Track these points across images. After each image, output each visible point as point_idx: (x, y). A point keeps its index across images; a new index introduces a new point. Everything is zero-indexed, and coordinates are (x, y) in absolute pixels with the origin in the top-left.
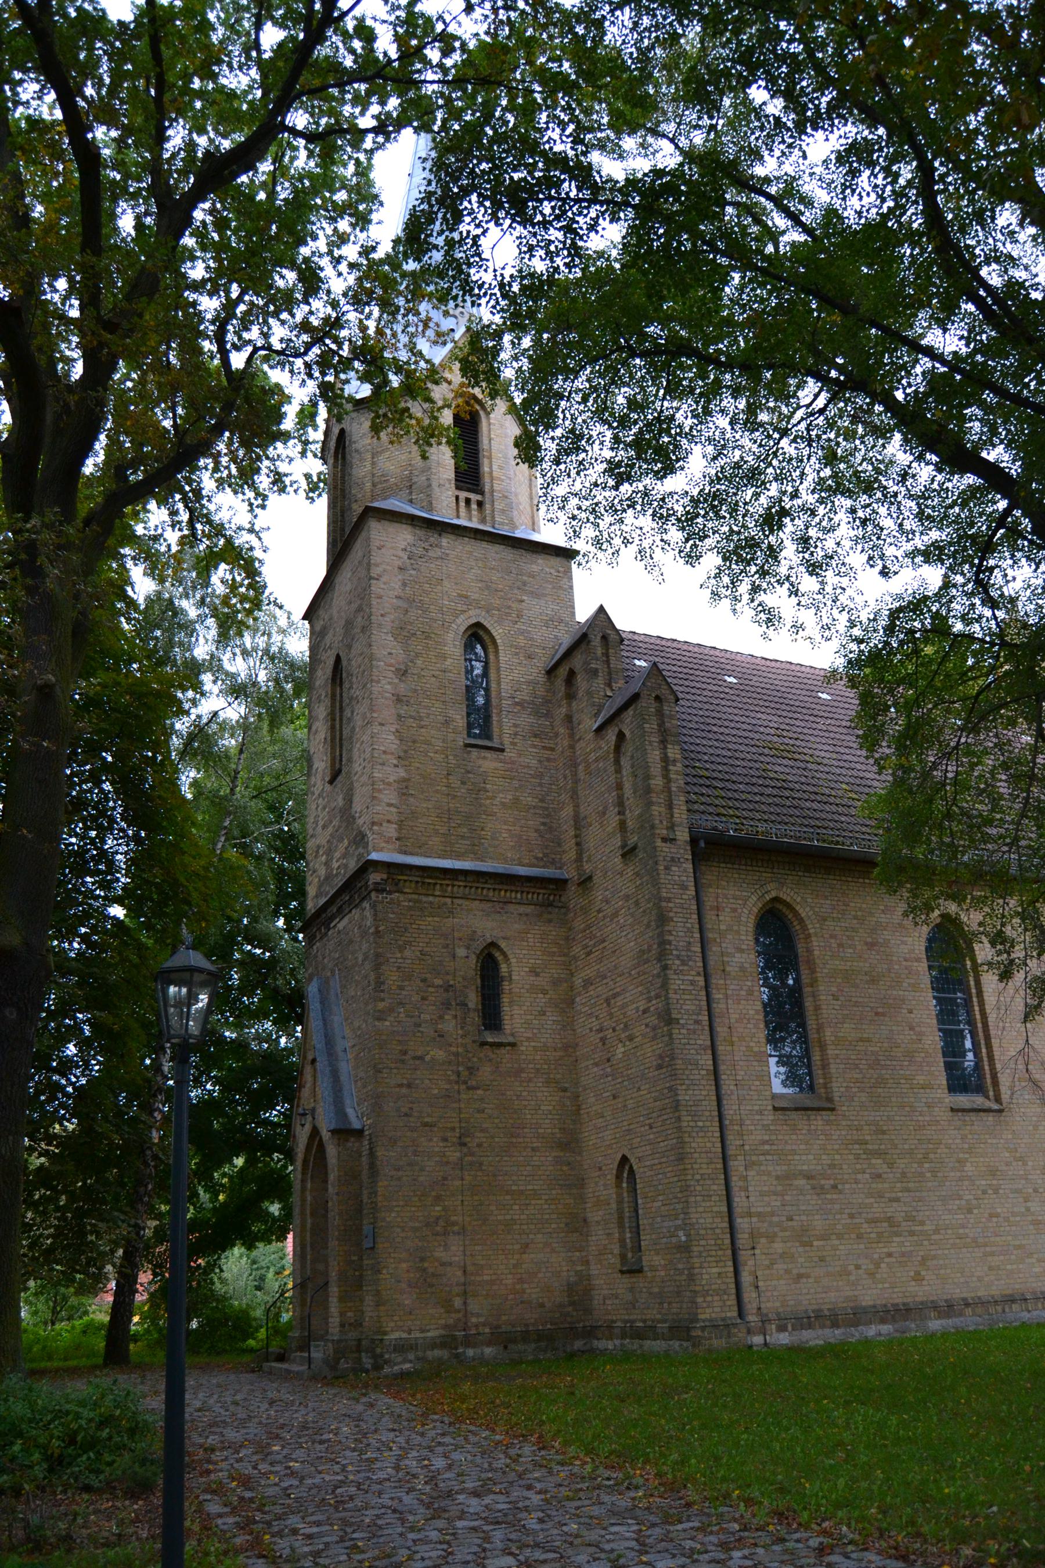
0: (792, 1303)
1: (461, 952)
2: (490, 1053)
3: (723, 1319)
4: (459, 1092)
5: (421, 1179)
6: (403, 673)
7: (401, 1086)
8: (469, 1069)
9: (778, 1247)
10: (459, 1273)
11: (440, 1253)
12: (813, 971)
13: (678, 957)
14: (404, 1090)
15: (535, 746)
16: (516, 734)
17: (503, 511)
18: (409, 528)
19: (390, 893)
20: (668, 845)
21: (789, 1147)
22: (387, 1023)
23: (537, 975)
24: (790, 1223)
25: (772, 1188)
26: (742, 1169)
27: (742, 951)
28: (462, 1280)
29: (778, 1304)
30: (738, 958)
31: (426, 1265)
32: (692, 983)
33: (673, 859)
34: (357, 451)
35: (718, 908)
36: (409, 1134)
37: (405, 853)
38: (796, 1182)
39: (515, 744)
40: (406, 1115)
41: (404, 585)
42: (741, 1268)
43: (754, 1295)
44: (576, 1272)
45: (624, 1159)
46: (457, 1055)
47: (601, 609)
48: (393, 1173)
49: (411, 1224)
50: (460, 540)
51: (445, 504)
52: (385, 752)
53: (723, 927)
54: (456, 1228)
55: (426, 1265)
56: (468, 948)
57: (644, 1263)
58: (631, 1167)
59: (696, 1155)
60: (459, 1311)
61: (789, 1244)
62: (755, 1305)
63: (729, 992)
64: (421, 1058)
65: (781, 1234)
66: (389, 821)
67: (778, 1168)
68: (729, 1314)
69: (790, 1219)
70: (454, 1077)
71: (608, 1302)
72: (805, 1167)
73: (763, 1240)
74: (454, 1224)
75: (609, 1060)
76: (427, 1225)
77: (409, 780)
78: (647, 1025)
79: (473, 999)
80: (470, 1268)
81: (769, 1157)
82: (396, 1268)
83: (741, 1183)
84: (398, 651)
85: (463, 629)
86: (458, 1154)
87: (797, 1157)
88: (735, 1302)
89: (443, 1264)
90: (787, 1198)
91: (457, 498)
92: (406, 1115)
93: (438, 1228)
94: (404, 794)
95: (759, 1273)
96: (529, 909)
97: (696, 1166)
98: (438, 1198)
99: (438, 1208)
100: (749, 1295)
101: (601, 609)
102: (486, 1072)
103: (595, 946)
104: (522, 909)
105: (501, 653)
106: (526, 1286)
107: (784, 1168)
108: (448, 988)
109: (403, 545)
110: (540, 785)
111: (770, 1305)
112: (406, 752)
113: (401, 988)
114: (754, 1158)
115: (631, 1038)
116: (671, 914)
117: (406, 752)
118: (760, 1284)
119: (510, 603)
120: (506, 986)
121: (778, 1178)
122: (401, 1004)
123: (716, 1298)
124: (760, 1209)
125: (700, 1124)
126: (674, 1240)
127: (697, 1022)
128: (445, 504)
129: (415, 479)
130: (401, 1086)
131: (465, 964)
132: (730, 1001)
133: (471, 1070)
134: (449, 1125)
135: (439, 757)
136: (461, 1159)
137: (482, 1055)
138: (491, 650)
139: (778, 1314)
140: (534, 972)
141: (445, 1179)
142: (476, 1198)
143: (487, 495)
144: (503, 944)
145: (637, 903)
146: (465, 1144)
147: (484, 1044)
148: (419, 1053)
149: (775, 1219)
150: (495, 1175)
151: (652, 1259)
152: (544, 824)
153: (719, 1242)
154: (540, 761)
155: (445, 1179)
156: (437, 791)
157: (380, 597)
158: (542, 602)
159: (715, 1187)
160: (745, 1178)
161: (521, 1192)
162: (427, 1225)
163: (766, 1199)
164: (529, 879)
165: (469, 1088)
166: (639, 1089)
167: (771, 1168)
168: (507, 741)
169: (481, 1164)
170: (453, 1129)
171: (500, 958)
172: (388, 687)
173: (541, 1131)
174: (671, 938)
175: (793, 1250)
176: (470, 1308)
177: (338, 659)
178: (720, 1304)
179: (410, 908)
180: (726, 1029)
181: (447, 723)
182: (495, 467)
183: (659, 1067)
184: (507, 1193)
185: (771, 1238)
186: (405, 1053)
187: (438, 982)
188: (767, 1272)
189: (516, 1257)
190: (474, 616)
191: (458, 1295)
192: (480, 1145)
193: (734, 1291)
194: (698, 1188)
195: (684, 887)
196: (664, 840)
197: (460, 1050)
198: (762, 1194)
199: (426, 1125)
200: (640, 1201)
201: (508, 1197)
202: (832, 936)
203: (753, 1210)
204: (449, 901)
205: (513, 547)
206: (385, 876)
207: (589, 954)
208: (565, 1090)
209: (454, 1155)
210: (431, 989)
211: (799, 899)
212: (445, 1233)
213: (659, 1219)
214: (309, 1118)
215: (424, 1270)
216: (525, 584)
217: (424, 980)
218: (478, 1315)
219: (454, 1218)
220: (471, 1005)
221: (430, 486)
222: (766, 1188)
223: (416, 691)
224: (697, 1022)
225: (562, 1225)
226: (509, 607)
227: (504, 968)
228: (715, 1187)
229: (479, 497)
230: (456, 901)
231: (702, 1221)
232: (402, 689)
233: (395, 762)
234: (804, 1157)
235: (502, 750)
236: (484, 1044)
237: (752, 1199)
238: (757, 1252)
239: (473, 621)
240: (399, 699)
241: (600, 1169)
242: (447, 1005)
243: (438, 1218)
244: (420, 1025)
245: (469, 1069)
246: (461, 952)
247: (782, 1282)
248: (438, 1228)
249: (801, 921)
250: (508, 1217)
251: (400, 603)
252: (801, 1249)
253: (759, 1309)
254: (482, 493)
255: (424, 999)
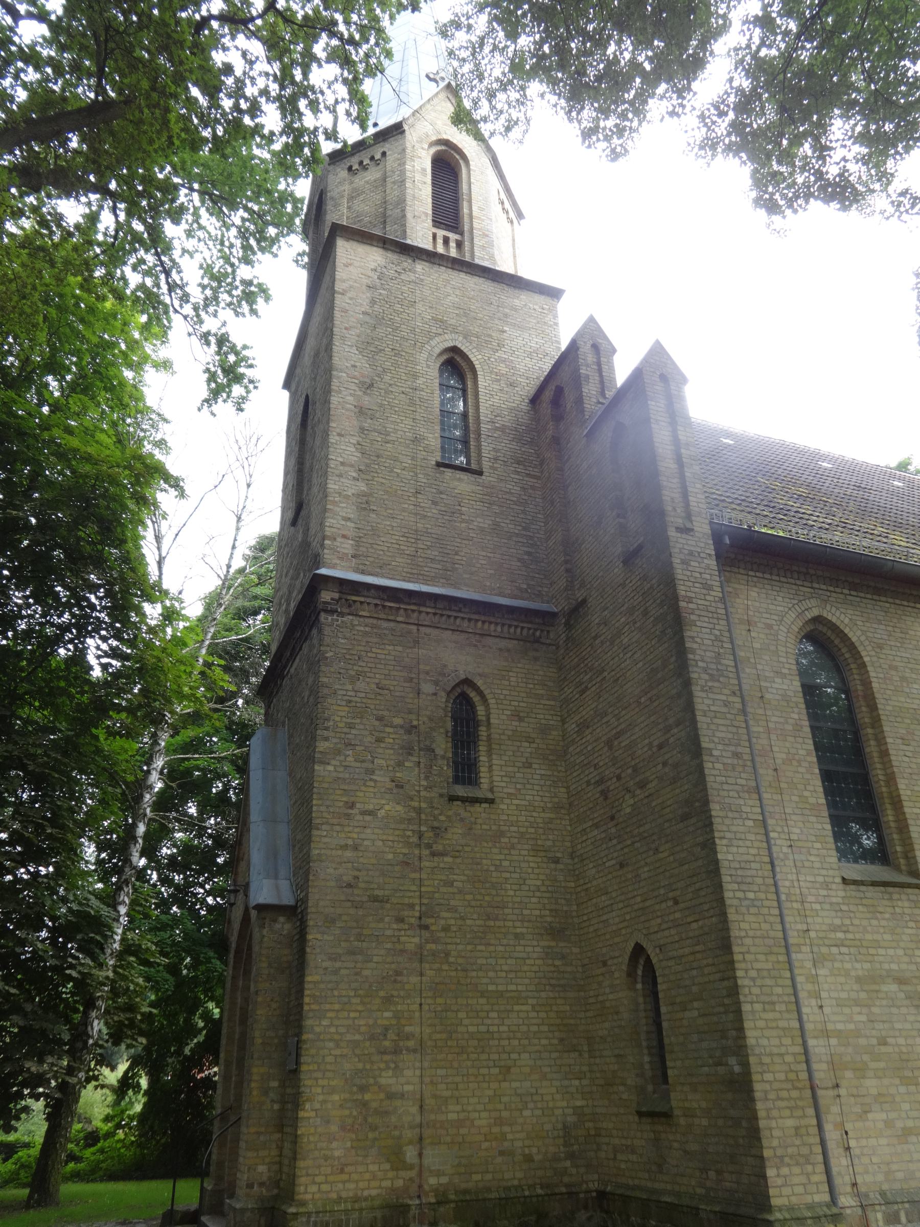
0: (900, 1175)
1: (427, 688)
2: (461, 811)
3: (810, 1207)
4: (420, 858)
5: (366, 973)
6: (368, 387)
7: (345, 847)
8: (433, 828)
9: (871, 1085)
10: (414, 1110)
11: (387, 1079)
12: (873, 707)
13: (705, 670)
14: (349, 854)
15: (518, 473)
16: (496, 459)
17: (483, 248)
18: (381, 251)
19: (342, 614)
20: (684, 536)
21: (869, 937)
22: (331, 768)
23: (521, 719)
24: (883, 1049)
25: (853, 995)
26: (809, 964)
27: (784, 676)
28: (418, 1119)
29: (880, 1177)
30: (779, 683)
31: (367, 1097)
32: (726, 704)
33: (691, 553)
34: (332, 198)
35: (749, 623)
36: (352, 911)
37: (363, 572)
38: (884, 988)
39: (495, 469)
40: (349, 886)
41: (373, 302)
42: (823, 1117)
43: (844, 1162)
44: (574, 1108)
45: (639, 950)
46: (419, 811)
47: (591, 320)
48: (327, 964)
49: (349, 1037)
50: (436, 268)
51: (420, 234)
52: (342, 464)
53: (757, 645)
54: (411, 1044)
55: (367, 1097)
56: (436, 683)
57: (674, 1103)
58: (648, 960)
59: (748, 941)
60: (411, 1167)
61: (886, 1081)
62: (847, 1179)
63: (771, 725)
64: (370, 813)
65: (873, 1065)
66: (344, 536)
67: (858, 966)
68: (817, 1198)
69: (883, 1042)
70: (415, 840)
71: (620, 1157)
72: (894, 966)
73: (849, 1074)
74: (408, 1037)
75: (612, 818)
76: (372, 1038)
77: (371, 495)
78: (665, 764)
79: (443, 746)
80: (430, 1102)
81: (844, 950)
82: (324, 1102)
83: (809, 987)
84: (363, 363)
85: (437, 351)
86: (416, 940)
87: (881, 951)
88: (824, 1178)
89: (390, 1096)
90: (875, 1010)
91: (434, 236)
92: (349, 886)
93: (387, 1043)
94: (365, 509)
95: (849, 1127)
96: (511, 644)
97: (748, 957)
98: (388, 1000)
99: (387, 1014)
100: (839, 1162)
101: (591, 320)
102: (455, 835)
103: (591, 680)
104: (503, 644)
105: (480, 378)
106: (506, 1129)
107: (867, 966)
108: (411, 729)
109: (373, 265)
110: (524, 512)
111: (871, 1179)
112: (367, 466)
113: (351, 726)
114: (824, 950)
115: (642, 785)
116: (693, 617)
117: (367, 466)
118: (852, 1143)
119: (490, 332)
120: (483, 732)
121: (858, 979)
122: (348, 745)
123: (796, 1170)
124: (840, 1026)
125: (751, 895)
126: (721, 1070)
127: (737, 755)
128: (420, 234)
129: (389, 213)
130: (345, 847)
131: (434, 705)
132: (773, 737)
133: (438, 831)
134: (406, 901)
135: (407, 475)
136: (421, 947)
137: (450, 813)
138: (469, 376)
139: (883, 1194)
140: (517, 716)
141: (398, 973)
142: (439, 1000)
143: (466, 234)
144: (479, 683)
145: (646, 613)
146: (426, 927)
147: (452, 799)
148: (371, 807)
149: (862, 1041)
150: (465, 970)
151: (684, 1099)
152: (529, 553)
153: (792, 1076)
154: (523, 489)
155: (398, 973)
156: (404, 510)
157: (346, 311)
158: (526, 335)
159: (779, 990)
160: (813, 979)
161: (501, 994)
162: (372, 1038)
163: (847, 1010)
164: (511, 610)
165: (433, 854)
166: (657, 850)
167: (848, 966)
168: (486, 465)
169: (447, 954)
170: (412, 906)
171: (477, 699)
172: (350, 398)
173: (526, 912)
174: (695, 646)
175: (892, 1090)
176: (426, 1161)
177: (307, 396)
178: (803, 1179)
179: (366, 633)
180: (771, 772)
181: (416, 440)
182: (474, 208)
183: (685, 817)
184: (483, 994)
185: (861, 1071)
186: (352, 806)
187: (398, 721)
188: (859, 1125)
189: (494, 1085)
190: (449, 340)
191: (410, 1143)
192: (446, 929)
193: (820, 1158)
194: (756, 991)
195: (709, 588)
196: (678, 529)
197: (423, 805)
198: (840, 1003)
199: (375, 899)
200: (663, 1009)
201: (483, 1001)
202: (892, 668)
203: (830, 1026)
204: (414, 628)
205: (494, 280)
206: (336, 596)
207: (583, 692)
208: (557, 861)
209: (412, 941)
210: (388, 730)
211: (847, 621)
212: (396, 1051)
213: (695, 1037)
214: (241, 896)
215: (365, 1104)
216: (506, 315)
217: (380, 719)
218: (439, 1173)
219: (408, 1029)
220: (440, 752)
221: (404, 216)
222: (844, 995)
223: (381, 405)
224: (737, 755)
225: (555, 1041)
226: (490, 336)
227: (481, 710)
228: (779, 990)
229: (457, 237)
230: (422, 629)
231: (764, 1042)
232: (366, 401)
233: (354, 474)
234: (891, 952)
235: (480, 473)
236: (452, 799)
237: (827, 1010)
238: (843, 1091)
239: (450, 344)
240: (361, 411)
241: (605, 964)
242: (409, 750)
243: (386, 1029)
244: (372, 772)
245: (433, 828)
246: (427, 688)
247: (883, 1141)
248: (387, 1043)
249: (852, 647)
250: (483, 1029)
251: (367, 319)
252: (902, 1089)
253: (854, 1185)
254: (462, 234)
255: (379, 740)
